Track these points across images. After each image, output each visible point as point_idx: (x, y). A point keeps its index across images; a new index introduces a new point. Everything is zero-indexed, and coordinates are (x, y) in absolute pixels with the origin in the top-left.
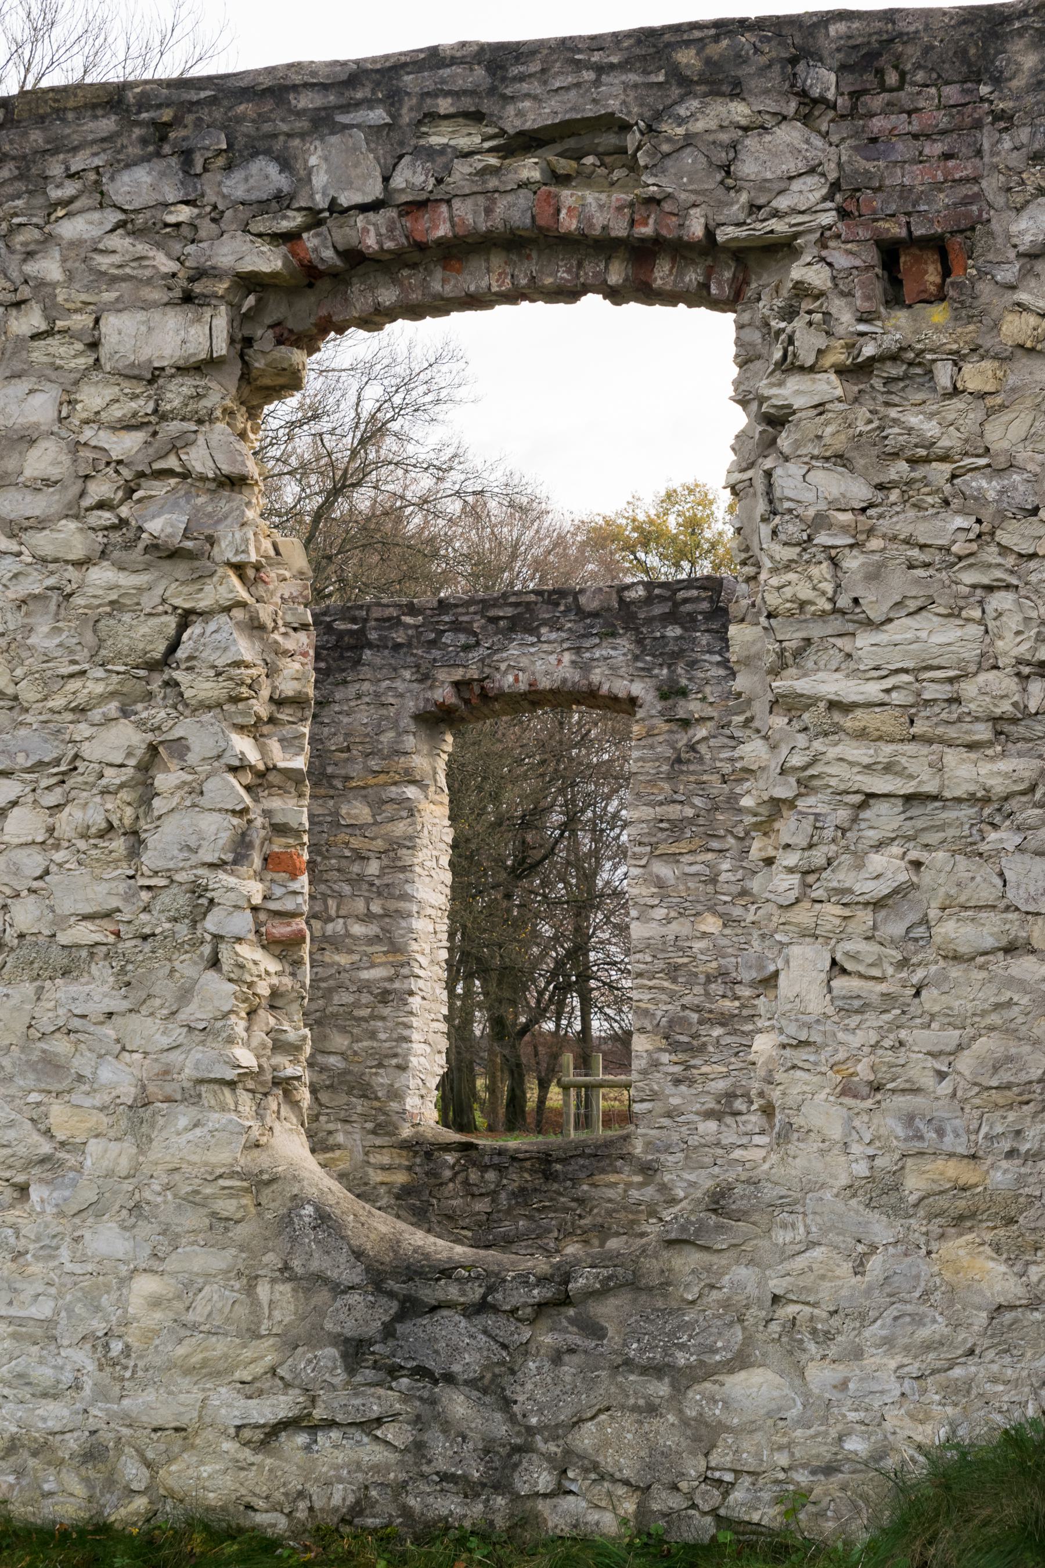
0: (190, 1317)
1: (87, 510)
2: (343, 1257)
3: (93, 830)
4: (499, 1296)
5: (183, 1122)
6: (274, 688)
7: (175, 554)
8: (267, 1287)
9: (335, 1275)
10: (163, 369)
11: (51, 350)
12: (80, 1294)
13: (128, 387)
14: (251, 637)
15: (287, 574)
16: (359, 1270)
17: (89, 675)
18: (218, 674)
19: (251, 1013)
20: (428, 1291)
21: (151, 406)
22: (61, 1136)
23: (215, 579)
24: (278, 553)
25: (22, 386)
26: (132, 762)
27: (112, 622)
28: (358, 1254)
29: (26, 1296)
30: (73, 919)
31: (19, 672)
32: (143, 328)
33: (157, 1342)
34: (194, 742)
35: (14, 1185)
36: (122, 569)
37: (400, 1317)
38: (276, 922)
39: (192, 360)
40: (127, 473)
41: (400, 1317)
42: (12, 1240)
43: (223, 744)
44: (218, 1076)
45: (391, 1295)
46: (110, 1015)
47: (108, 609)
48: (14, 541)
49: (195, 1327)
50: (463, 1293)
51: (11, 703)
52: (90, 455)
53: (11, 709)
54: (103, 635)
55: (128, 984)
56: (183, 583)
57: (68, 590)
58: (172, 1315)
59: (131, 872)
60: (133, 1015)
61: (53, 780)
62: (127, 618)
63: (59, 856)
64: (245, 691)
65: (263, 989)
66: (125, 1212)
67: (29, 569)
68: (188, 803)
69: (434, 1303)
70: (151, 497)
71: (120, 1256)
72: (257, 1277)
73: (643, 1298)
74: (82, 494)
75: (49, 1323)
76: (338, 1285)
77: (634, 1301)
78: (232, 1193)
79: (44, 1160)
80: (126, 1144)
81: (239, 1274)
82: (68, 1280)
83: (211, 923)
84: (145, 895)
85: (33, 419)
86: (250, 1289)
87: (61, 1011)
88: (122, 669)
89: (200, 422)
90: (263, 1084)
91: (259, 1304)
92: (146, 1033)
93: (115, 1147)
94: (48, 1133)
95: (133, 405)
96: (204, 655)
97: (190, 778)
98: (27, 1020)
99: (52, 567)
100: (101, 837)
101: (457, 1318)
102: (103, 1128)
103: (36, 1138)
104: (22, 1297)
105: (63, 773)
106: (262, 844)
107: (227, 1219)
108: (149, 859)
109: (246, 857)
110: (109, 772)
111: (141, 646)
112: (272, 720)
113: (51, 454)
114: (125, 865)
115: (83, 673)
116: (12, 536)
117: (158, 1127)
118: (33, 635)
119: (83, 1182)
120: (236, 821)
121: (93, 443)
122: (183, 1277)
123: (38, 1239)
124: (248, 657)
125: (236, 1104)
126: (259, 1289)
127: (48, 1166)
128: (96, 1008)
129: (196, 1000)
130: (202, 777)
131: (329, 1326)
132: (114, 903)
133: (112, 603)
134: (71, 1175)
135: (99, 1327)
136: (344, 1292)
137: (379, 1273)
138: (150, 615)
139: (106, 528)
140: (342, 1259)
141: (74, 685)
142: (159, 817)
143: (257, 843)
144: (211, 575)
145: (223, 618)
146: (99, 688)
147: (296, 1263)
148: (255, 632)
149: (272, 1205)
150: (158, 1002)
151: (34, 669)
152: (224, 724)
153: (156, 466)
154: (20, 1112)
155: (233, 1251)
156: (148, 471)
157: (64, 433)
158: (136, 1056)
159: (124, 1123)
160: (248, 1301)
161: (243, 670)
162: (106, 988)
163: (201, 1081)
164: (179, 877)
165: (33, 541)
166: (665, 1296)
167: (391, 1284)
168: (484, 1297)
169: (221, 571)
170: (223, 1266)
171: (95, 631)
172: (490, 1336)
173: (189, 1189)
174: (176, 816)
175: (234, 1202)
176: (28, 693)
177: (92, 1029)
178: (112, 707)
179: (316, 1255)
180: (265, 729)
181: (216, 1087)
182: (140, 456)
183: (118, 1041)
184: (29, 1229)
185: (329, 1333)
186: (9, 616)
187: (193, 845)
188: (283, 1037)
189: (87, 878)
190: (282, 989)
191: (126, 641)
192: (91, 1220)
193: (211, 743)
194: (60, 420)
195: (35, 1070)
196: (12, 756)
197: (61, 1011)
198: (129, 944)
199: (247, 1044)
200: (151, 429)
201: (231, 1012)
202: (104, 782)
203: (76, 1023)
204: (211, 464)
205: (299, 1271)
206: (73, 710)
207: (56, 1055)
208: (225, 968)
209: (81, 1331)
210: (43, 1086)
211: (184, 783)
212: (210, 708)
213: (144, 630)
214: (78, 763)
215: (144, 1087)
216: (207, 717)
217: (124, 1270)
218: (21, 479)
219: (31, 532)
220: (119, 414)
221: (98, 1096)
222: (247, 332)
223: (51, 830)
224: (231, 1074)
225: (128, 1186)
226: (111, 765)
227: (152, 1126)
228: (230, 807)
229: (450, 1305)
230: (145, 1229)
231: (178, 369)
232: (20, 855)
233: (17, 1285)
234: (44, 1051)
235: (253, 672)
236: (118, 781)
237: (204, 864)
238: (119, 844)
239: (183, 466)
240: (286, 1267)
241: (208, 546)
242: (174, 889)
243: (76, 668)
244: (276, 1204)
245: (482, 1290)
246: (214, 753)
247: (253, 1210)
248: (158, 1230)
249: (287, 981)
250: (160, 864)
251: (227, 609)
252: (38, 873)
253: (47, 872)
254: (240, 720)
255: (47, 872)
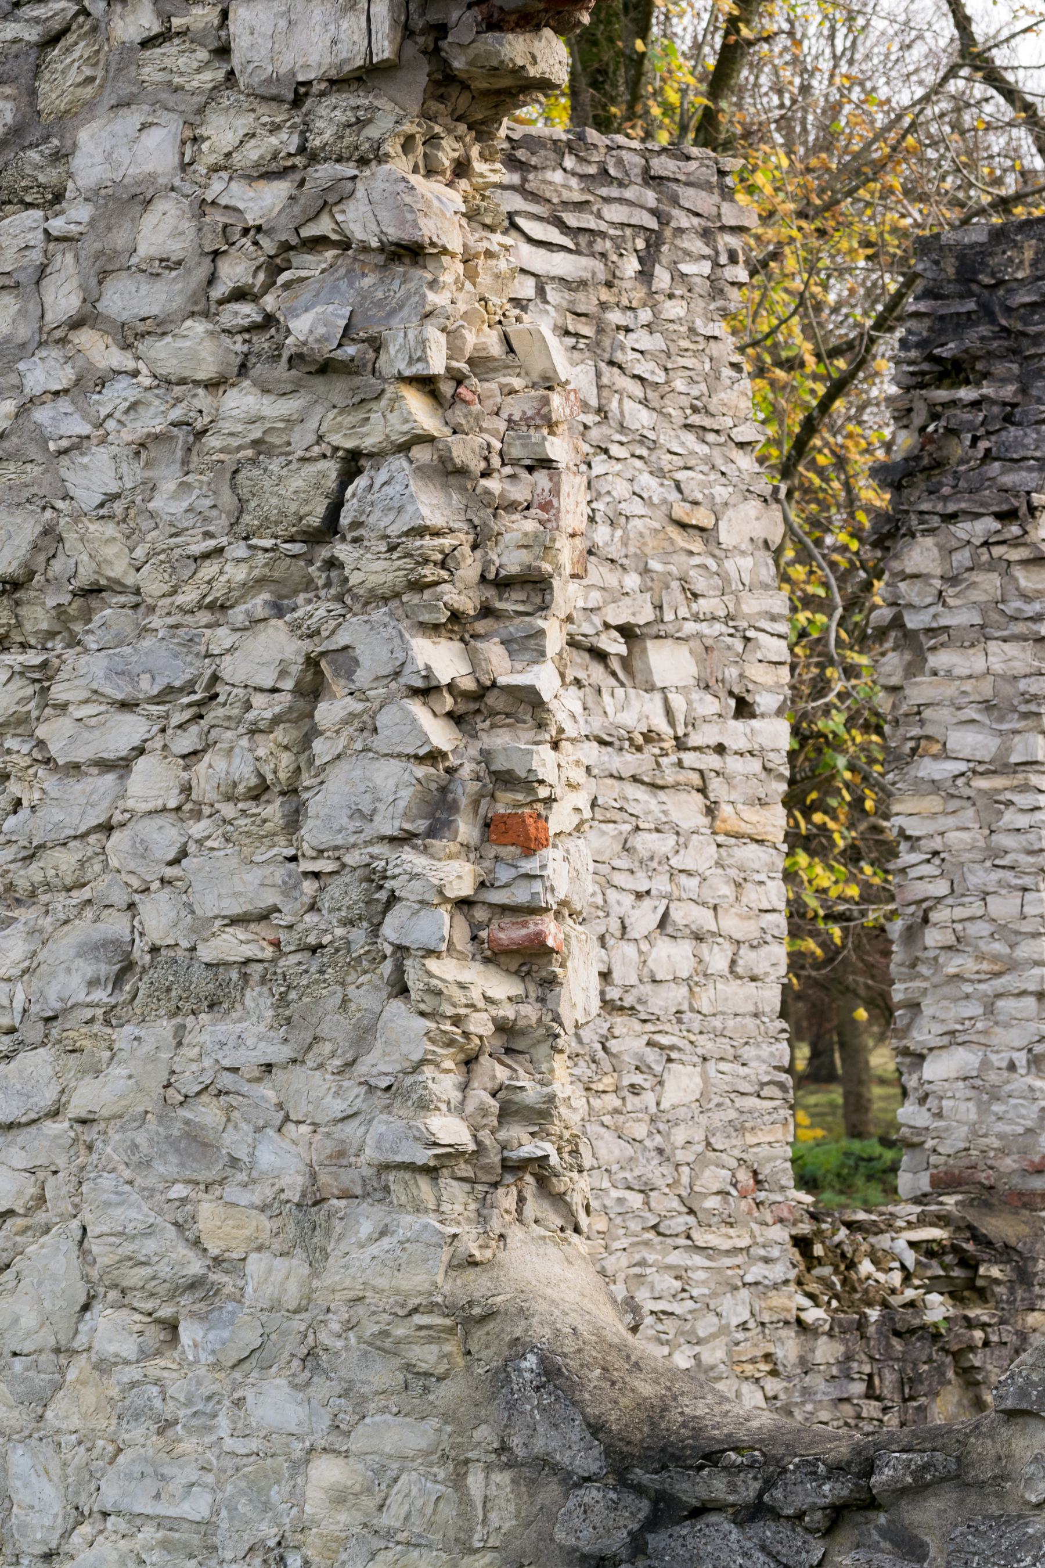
0: (386, 1520)
1: (221, 302)
2: (576, 1433)
3: (241, 789)
4: (778, 1493)
5: (366, 1228)
6: (487, 563)
7: (326, 368)
8: (481, 1476)
9: (567, 1461)
10: (308, 84)
11: (168, 62)
12: (243, 1484)
13: (268, 113)
14: (445, 487)
15: (517, 383)
16: (595, 1452)
17: (227, 554)
18: (392, 549)
19: (469, 1062)
20: (686, 1486)
21: (295, 140)
22: (214, 1251)
23: (384, 402)
24: (511, 350)
25: (134, 118)
26: (288, 684)
27: (256, 472)
28: (596, 1428)
29: (175, 1487)
30: (218, 923)
31: (140, 553)
32: (283, 24)
33: (344, 1556)
34: (361, 652)
35: (158, 1321)
36: (266, 391)
37: (652, 1524)
38: (507, 920)
39: (347, 68)
40: (269, 245)
41: (652, 1524)
42: (157, 1403)
43: (400, 655)
44: (407, 1159)
45: (639, 1490)
46: (269, 1067)
47: (249, 453)
48: (129, 354)
49: (389, 1534)
50: (733, 1489)
51: (134, 599)
52: (221, 218)
53: (136, 607)
54: (244, 493)
55: (289, 1020)
56: (343, 410)
57: (198, 426)
58: (359, 1517)
59: (290, 852)
60: (298, 1067)
61: (187, 715)
62: (274, 465)
63: (198, 829)
64: (430, 573)
65: (481, 1025)
66: (296, 1363)
67: (149, 395)
68: (358, 746)
69: (695, 1503)
70: (302, 280)
71: (293, 1429)
72: (467, 1462)
73: (972, 1499)
74: (212, 280)
75: (206, 1526)
76: (570, 1474)
77: (961, 1502)
78: (432, 1335)
79: (194, 1284)
80: (295, 1262)
81: (444, 1457)
82: (228, 1463)
83: (391, 929)
84: (309, 887)
85: (148, 168)
86: (458, 1481)
87: (207, 1062)
88: (268, 543)
89: (363, 162)
90: (488, 1169)
91: (470, 1503)
92: (314, 1094)
93: (281, 1264)
94: (197, 1243)
95: (274, 140)
96: (372, 520)
97: (358, 707)
98: (164, 1077)
99: (178, 390)
100: (256, 798)
101: (727, 1526)
102: (264, 1237)
103: (183, 1251)
104: (171, 1488)
105: (199, 704)
106: (476, 803)
107: (427, 1374)
108: (312, 833)
109: (448, 824)
110: (259, 700)
111: (293, 508)
112: (486, 611)
113: (170, 221)
114: (281, 840)
115: (219, 551)
116: (127, 347)
117: (335, 1236)
118: (157, 495)
119: (242, 1317)
120: (421, 771)
121: (223, 201)
122: (372, 1460)
123: (189, 1403)
124: (435, 518)
125: (439, 1201)
126: (470, 1480)
127: (200, 1293)
128: (250, 1057)
129: (379, 1044)
130: (376, 705)
131: (560, 1536)
132: (271, 898)
133: (255, 443)
134: (230, 1306)
135: (269, 1533)
136: (577, 1486)
137: (624, 1456)
138: (303, 459)
139: (247, 330)
140: (575, 1437)
141: (208, 570)
142: (323, 768)
143: (464, 802)
144: (378, 397)
145: (398, 462)
146: (239, 574)
147: (515, 1442)
148: (452, 480)
149: (484, 1354)
150: (327, 1048)
151: (160, 547)
152: (406, 623)
153: (306, 232)
154: (160, 1213)
155: (434, 1422)
156: (294, 241)
157: (188, 189)
158: (304, 1129)
159: (292, 1231)
160: (455, 1497)
161: (427, 541)
162: (262, 1028)
163: (387, 1167)
164: (352, 859)
165: (152, 354)
166: (1000, 1495)
167: (639, 1475)
168: (760, 1495)
169: (390, 389)
170: (423, 1444)
171: (234, 487)
172: (769, 1554)
173: (376, 1328)
174: (344, 765)
175: (434, 1348)
176: (153, 583)
177: (245, 1088)
178: (259, 603)
179: (541, 1430)
180: (480, 627)
181: (408, 1176)
182: (283, 220)
183: (280, 1106)
184: (177, 1389)
185: (561, 1547)
186: (125, 468)
187: (367, 810)
188: (518, 1097)
189: (234, 861)
190: (522, 1023)
191: (274, 501)
192: (255, 1374)
193: (385, 654)
194: (184, 167)
195: (177, 1150)
196: (134, 679)
197: (207, 1062)
198: (294, 959)
199: (460, 1109)
200: (297, 176)
201: (423, 1062)
202: (250, 716)
203: (227, 1080)
204: (374, 227)
205: (520, 1452)
206: (210, 607)
207: (203, 1128)
208: (414, 995)
209: (248, 1539)
210: (188, 1174)
211: (352, 715)
212: (385, 599)
213: (296, 483)
214: (219, 688)
215: (313, 1176)
216: (379, 614)
217: (298, 1448)
218: (134, 260)
219: (149, 340)
220: (254, 155)
221: (258, 1188)
222: (434, 16)
223: (187, 789)
224: (423, 1156)
225: (298, 1324)
226: (261, 690)
227: (328, 1234)
228: (410, 750)
229: (719, 1507)
230: (323, 1388)
231: (332, 82)
232: (148, 828)
233: (166, 1470)
234: (187, 1122)
235: (447, 542)
236: (268, 714)
237: (382, 838)
238: (274, 810)
239: (340, 231)
240: (504, 1448)
241: (371, 355)
242: (346, 878)
243: (212, 543)
244: (490, 1352)
245: (757, 1485)
246: (388, 669)
247: (460, 1361)
248: (338, 1390)
249: (530, 1012)
250: (326, 839)
251: (404, 448)
252: (171, 855)
253: (183, 854)
254: (426, 617)
255: (183, 854)
